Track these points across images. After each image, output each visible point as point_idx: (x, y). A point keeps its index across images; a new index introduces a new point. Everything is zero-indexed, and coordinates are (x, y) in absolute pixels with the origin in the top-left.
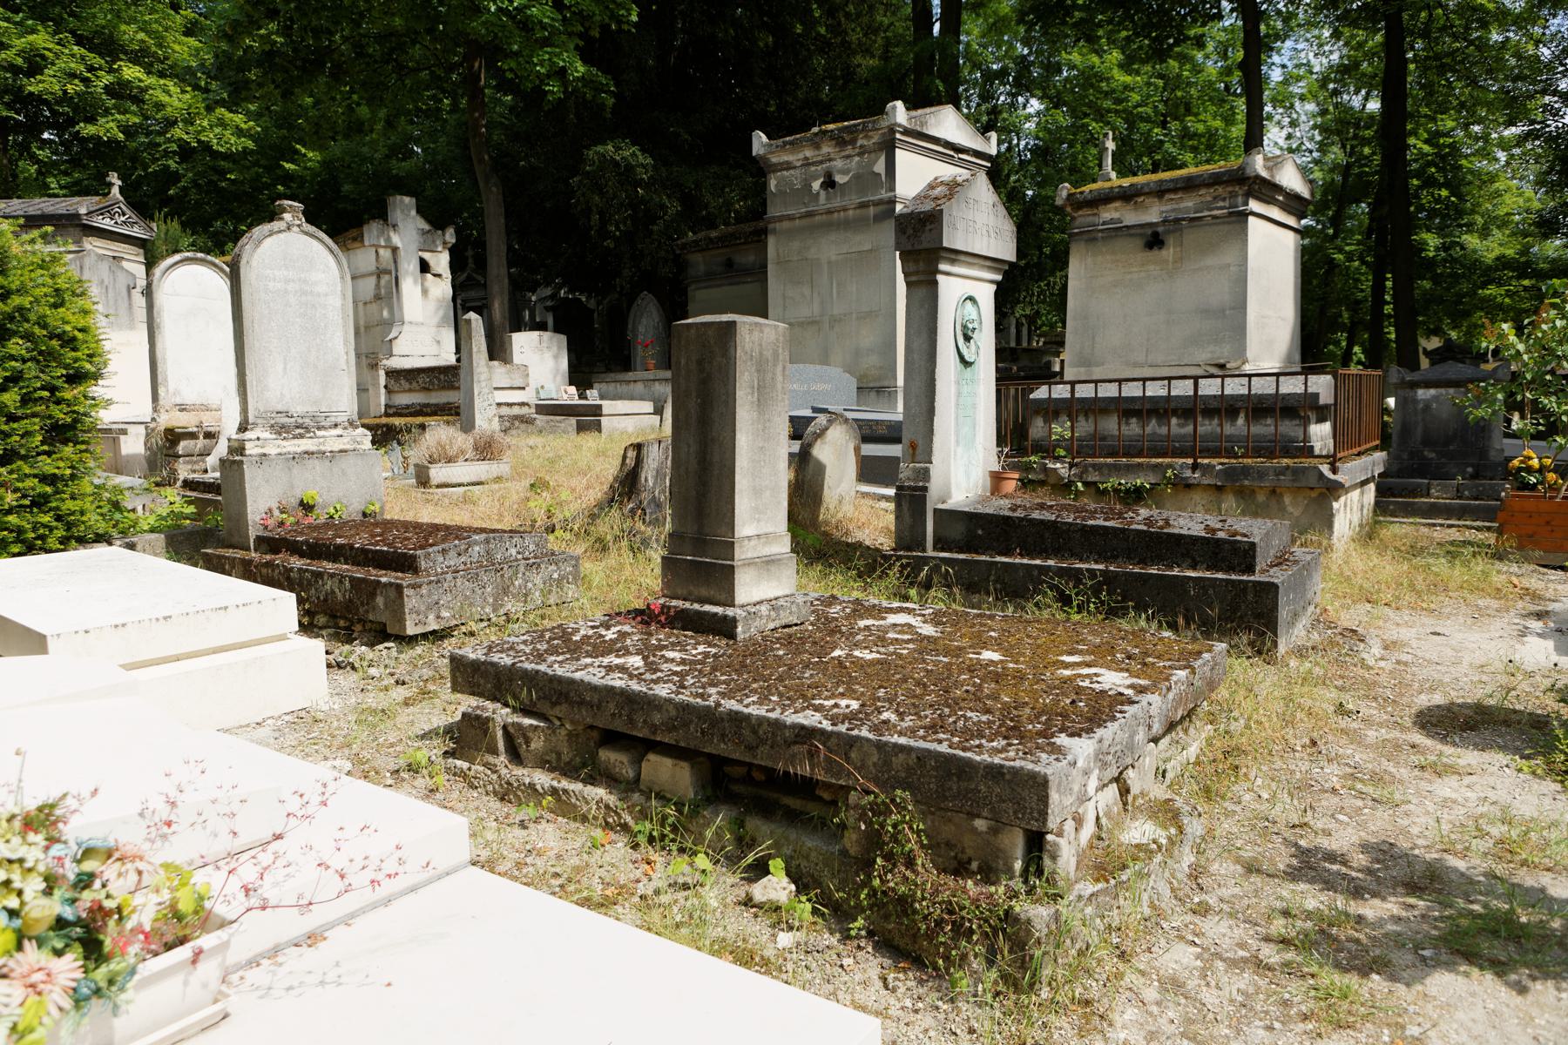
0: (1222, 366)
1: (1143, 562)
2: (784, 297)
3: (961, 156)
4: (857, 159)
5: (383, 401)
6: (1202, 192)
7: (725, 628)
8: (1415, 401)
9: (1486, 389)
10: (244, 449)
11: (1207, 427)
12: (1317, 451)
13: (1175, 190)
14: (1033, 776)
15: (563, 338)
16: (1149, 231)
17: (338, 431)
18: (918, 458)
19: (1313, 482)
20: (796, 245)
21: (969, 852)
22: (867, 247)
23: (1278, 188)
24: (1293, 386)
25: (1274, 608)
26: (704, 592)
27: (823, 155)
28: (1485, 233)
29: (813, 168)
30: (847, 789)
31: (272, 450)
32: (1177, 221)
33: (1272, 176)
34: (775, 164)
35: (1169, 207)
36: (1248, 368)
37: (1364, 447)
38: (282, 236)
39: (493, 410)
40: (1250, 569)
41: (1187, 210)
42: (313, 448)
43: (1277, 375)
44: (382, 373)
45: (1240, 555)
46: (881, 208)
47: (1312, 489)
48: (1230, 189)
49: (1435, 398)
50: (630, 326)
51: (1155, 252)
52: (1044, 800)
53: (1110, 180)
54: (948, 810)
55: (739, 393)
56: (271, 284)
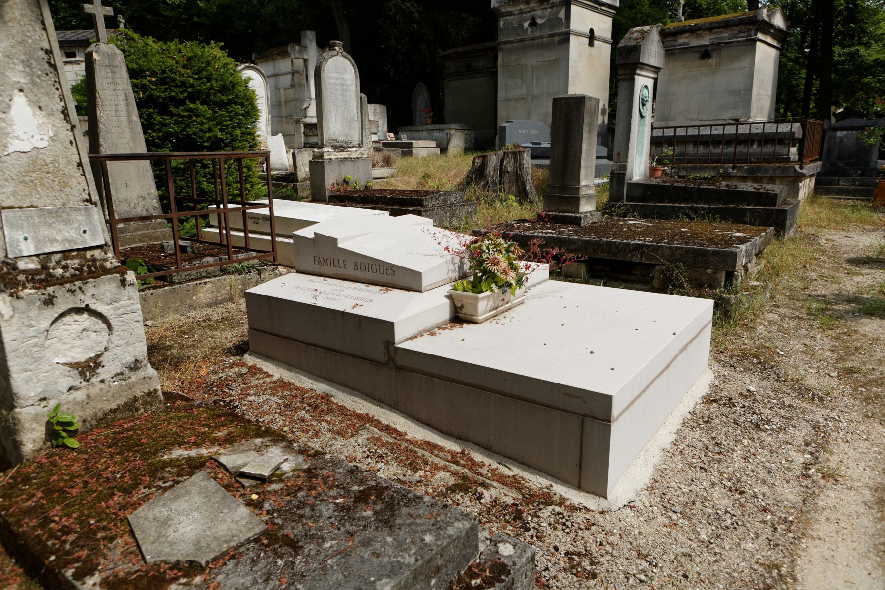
0: (737, 120)
1: (725, 203)
2: (507, 85)
3: (602, 8)
4: (549, 10)
5: (303, 140)
6: (733, 28)
7: (576, 222)
8: (835, 137)
9: (873, 130)
10: (323, 156)
11: (741, 149)
12: (791, 160)
13: (718, 28)
14: (731, 252)
15: (385, 108)
16: (703, 49)
17: (355, 149)
18: (621, 160)
19: (791, 173)
20: (513, 57)
21: (704, 281)
22: (553, 58)
23: (772, 26)
24: (771, 128)
25: (785, 220)
26: (564, 208)
27: (530, 8)
28: (867, 45)
29: (524, 15)
30: (654, 266)
31: (333, 157)
32: (719, 44)
33: (770, 20)
34: (503, 13)
35: (715, 37)
36: (750, 121)
37: (814, 158)
38: (335, 57)
39: (371, 144)
40: (774, 205)
41: (724, 38)
42: (347, 157)
43: (764, 123)
44: (302, 126)
45: (771, 199)
46: (560, 38)
47: (790, 177)
48: (748, 27)
49: (845, 136)
50: (413, 102)
51: (706, 60)
52: (735, 261)
53: (681, 21)
54: (696, 268)
55: (584, 127)
56: (331, 80)
